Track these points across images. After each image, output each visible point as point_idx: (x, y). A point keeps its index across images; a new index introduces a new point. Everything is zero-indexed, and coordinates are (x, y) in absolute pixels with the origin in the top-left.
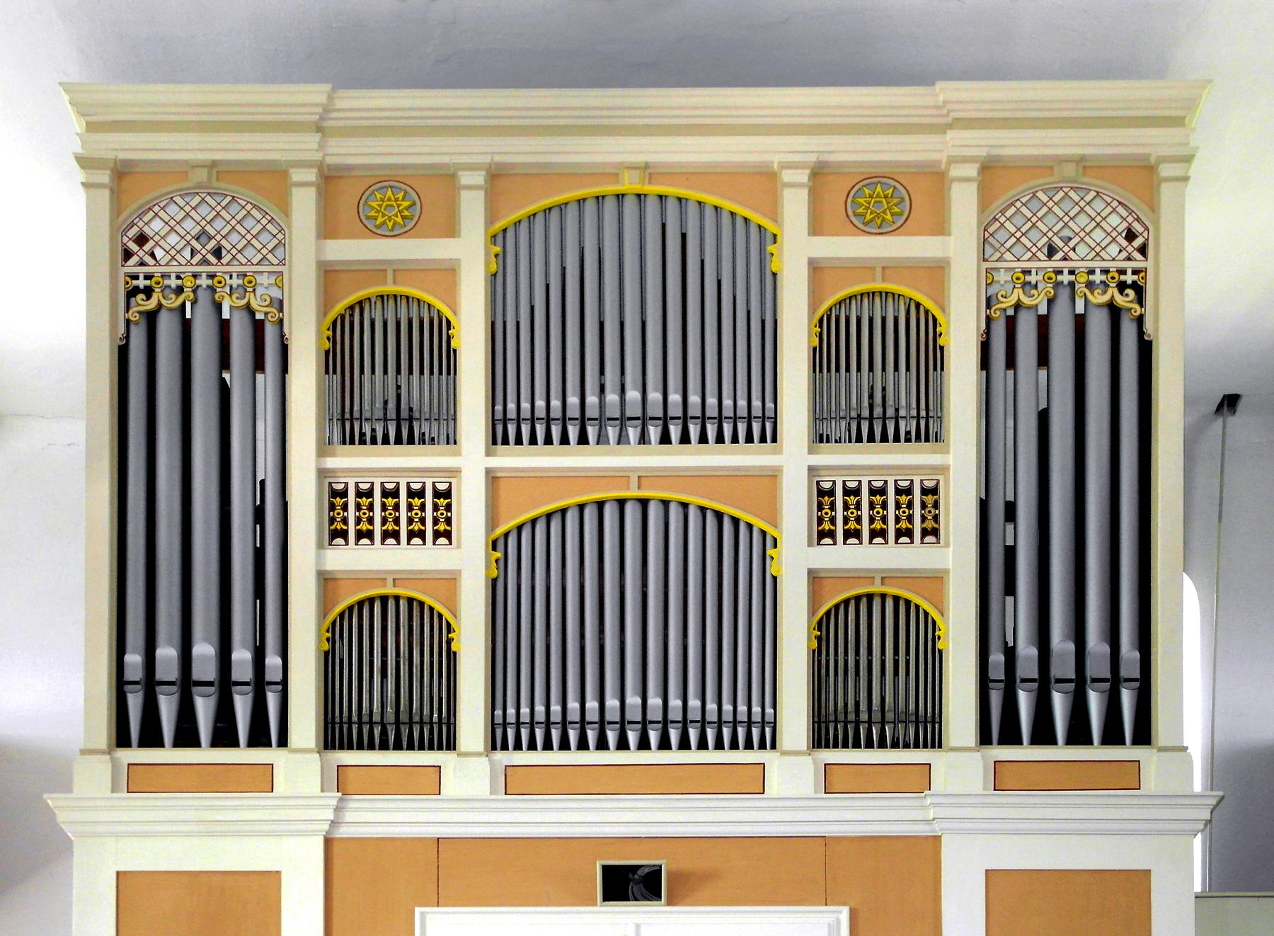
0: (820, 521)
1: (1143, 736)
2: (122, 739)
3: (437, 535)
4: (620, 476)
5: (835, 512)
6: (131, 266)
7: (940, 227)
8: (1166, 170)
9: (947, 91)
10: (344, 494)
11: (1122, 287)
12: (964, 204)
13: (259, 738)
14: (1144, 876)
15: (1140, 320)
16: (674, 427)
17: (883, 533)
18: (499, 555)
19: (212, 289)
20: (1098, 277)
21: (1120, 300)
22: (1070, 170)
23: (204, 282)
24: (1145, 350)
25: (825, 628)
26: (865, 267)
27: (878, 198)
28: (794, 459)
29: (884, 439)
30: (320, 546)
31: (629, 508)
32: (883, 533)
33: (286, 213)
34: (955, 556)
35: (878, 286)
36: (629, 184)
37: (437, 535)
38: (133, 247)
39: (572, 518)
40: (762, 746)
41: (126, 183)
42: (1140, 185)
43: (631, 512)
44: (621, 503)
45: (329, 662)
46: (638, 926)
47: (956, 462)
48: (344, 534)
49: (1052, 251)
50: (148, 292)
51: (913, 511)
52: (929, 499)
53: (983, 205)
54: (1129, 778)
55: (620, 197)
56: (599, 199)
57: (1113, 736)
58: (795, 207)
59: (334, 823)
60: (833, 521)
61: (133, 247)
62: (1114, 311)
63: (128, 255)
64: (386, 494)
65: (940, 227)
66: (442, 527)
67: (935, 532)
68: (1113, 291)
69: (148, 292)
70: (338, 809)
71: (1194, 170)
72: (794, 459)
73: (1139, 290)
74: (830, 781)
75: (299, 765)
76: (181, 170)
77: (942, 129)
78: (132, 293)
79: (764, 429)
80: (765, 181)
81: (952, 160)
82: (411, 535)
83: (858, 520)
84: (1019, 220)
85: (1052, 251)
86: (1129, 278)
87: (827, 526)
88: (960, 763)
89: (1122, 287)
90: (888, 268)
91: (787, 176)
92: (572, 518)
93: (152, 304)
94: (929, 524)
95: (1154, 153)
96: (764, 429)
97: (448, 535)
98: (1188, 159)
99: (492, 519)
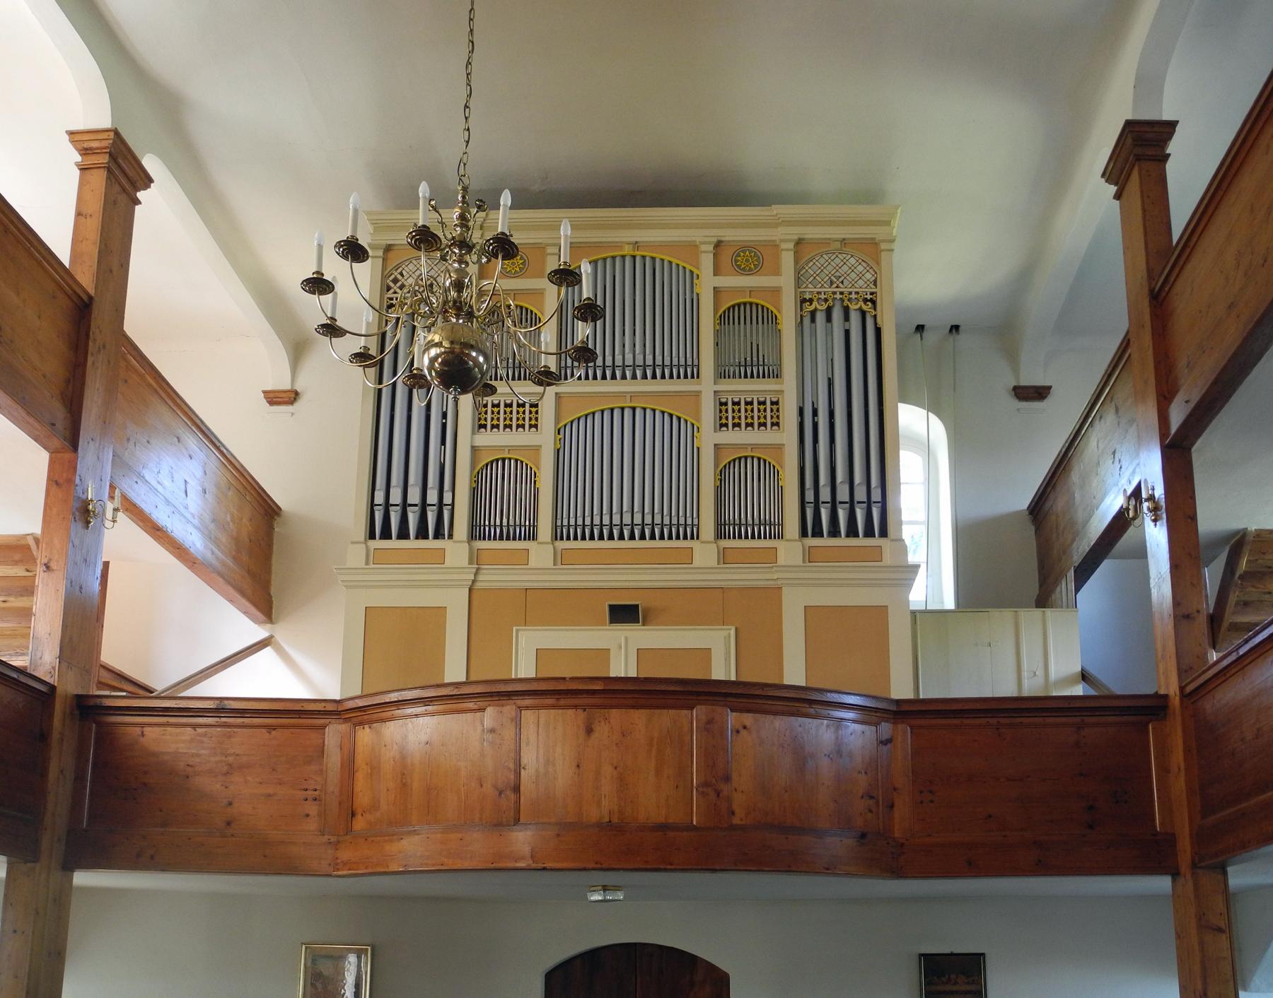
0: (721, 418)
1: (884, 533)
2: (372, 536)
3: (531, 426)
4: (633, 395)
5: (730, 414)
6: (390, 294)
7: (777, 272)
8: (883, 246)
9: (777, 210)
10: (726, 404)
11: (865, 300)
12: (787, 260)
13: (438, 535)
14: (884, 609)
15: (875, 316)
16: (654, 371)
17: (752, 425)
18: (561, 436)
19: (842, 300)
20: (853, 296)
21: (865, 308)
22: (838, 245)
23: (838, 296)
24: (878, 331)
25: (722, 476)
26: (741, 290)
27: (748, 258)
28: (707, 386)
29: (746, 376)
30: (473, 433)
31: (626, 412)
32: (752, 425)
33: (878, 263)
34: (787, 436)
35: (748, 299)
36: (627, 250)
37: (531, 426)
38: (392, 284)
39: (598, 416)
40: (692, 538)
41: (391, 255)
42: (872, 251)
43: (627, 413)
44: (623, 409)
45: (474, 492)
46: (626, 639)
47: (787, 390)
48: (485, 426)
49: (832, 283)
50: (811, 301)
51: (764, 413)
52: (775, 407)
53: (796, 261)
54: (877, 554)
55: (623, 257)
56: (614, 258)
57: (869, 533)
58: (707, 261)
59: (474, 581)
60: (727, 418)
61: (392, 284)
62: (863, 313)
63: (389, 288)
64: (734, 404)
65: (777, 272)
66: (533, 422)
67: (777, 424)
68: (861, 303)
69: (811, 301)
70: (476, 574)
71: (895, 246)
72: (707, 386)
73: (874, 302)
74: (724, 557)
75: (456, 550)
76: (826, 242)
77: (776, 225)
78: (803, 301)
79: (692, 372)
80: (692, 249)
81: (782, 241)
82: (518, 426)
83: (740, 418)
84: (815, 268)
85: (832, 283)
86: (869, 297)
87: (724, 421)
88: (790, 549)
89: (865, 300)
90: (752, 291)
91: (783, 246)
92: (598, 416)
93: (812, 308)
94: (775, 420)
95: (878, 238)
96: (692, 372)
97: (536, 426)
98: (893, 241)
99: (557, 420)
